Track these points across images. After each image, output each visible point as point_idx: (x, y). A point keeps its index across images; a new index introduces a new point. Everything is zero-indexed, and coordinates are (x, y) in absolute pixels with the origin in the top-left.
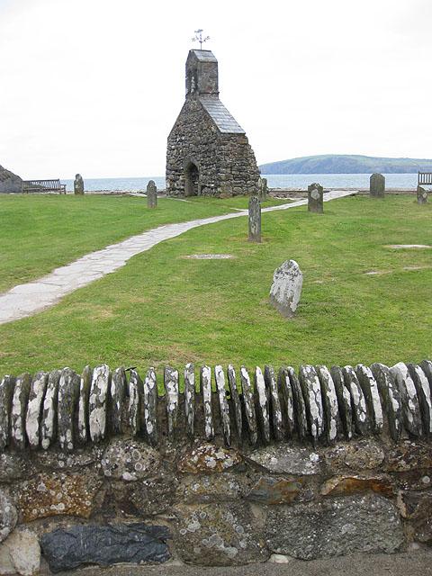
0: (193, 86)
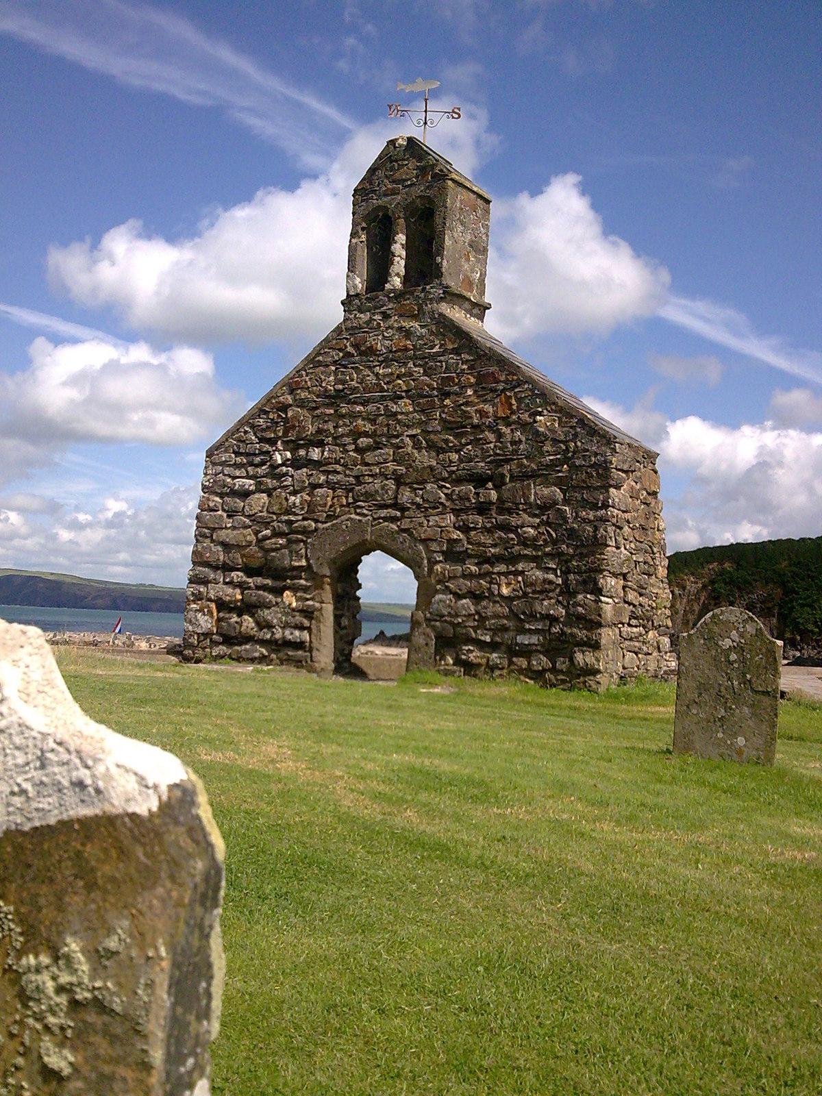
0: (399, 265)
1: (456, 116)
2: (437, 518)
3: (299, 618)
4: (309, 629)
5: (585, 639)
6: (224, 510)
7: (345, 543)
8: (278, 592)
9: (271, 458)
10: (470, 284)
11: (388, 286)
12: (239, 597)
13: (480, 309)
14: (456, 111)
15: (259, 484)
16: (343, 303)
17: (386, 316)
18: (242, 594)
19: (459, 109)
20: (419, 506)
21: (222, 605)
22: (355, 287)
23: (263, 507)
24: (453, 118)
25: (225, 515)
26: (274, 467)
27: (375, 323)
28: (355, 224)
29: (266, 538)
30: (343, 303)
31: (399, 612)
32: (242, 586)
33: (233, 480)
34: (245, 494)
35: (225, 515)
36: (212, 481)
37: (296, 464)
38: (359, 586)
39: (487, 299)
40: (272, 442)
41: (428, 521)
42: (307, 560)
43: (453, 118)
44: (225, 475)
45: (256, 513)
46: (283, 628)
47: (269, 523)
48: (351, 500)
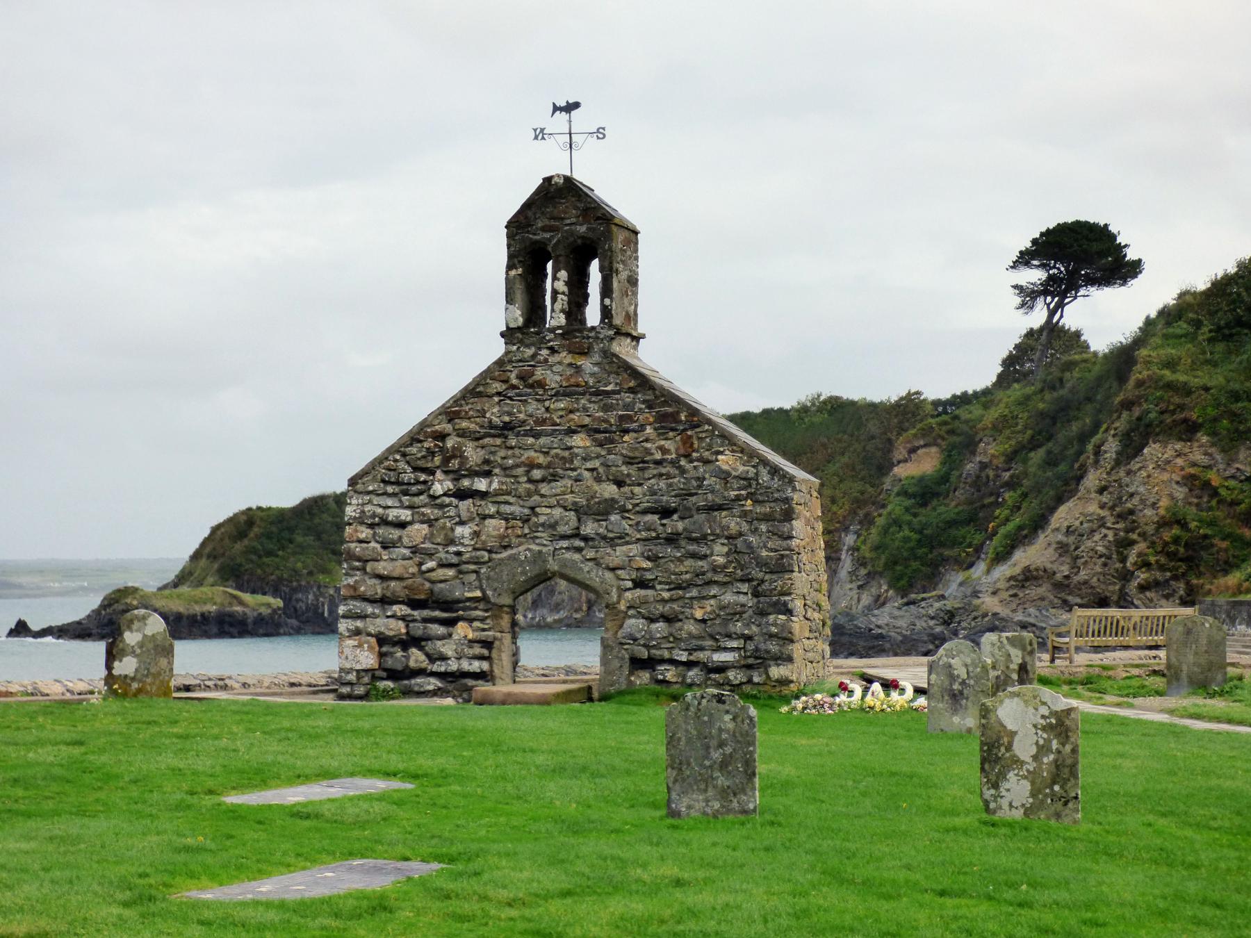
1: (601, 136)
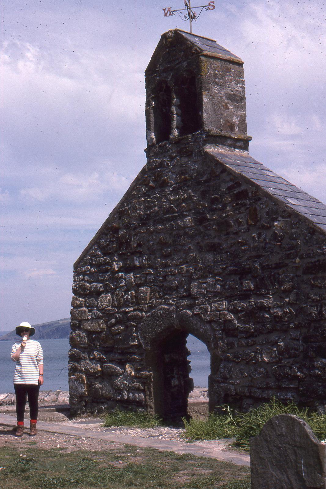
2: (216, 305)
3: (137, 384)
4: (144, 391)
5: (235, 416)
6: (86, 307)
7: (160, 326)
8: (122, 364)
9: (111, 267)
10: (231, 127)
11: (171, 136)
12: (99, 369)
13: (244, 144)
14: (211, 4)
15: (105, 286)
16: (145, 151)
17: (172, 158)
18: (101, 367)
19: (213, 2)
20: (204, 295)
21: (90, 375)
22: (152, 139)
23: (308, 256)
24: (210, 9)
25: (87, 310)
26: (114, 272)
27: (166, 163)
28: (148, 95)
29: (113, 325)
30: (145, 151)
31: (48, 415)
32: (100, 361)
33: (90, 284)
34: (98, 294)
35: (87, 310)
36: (78, 286)
37: (127, 269)
38: (188, 353)
39: (249, 135)
40: (111, 255)
41: (211, 307)
42: (139, 340)
43: (210, 9)
44: (85, 281)
45: (105, 307)
46: (129, 392)
47: (113, 314)
48: (161, 294)
